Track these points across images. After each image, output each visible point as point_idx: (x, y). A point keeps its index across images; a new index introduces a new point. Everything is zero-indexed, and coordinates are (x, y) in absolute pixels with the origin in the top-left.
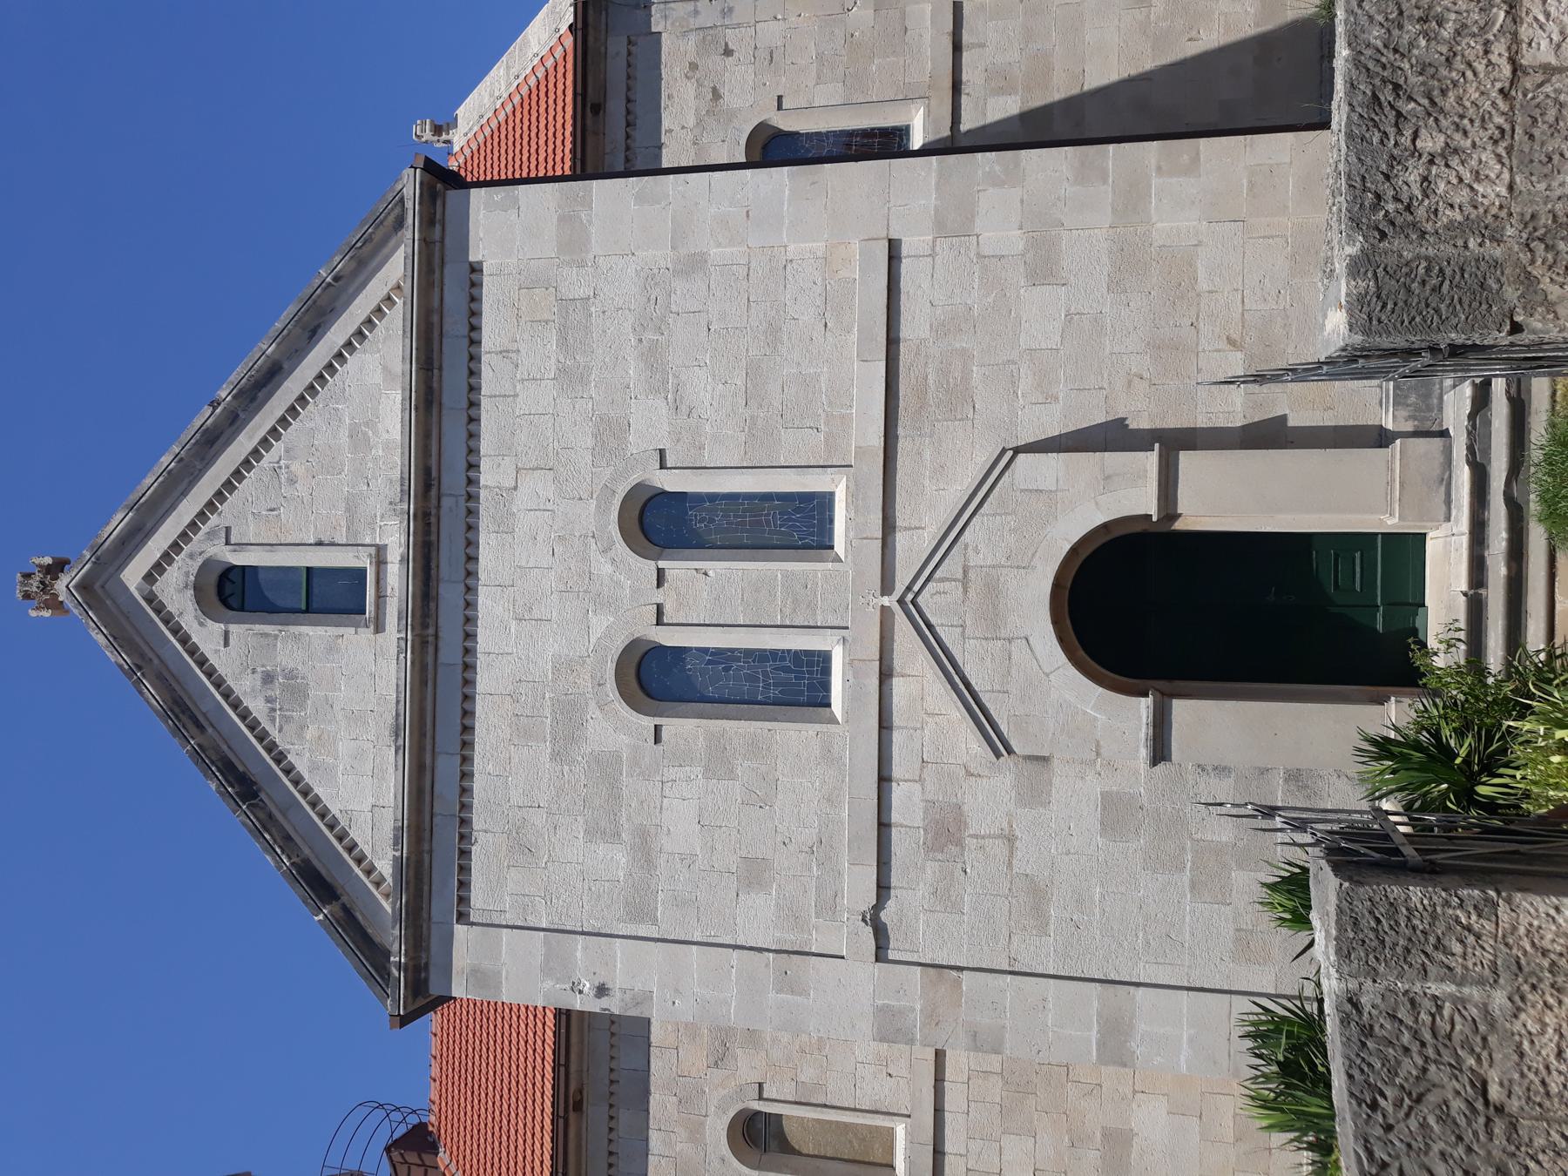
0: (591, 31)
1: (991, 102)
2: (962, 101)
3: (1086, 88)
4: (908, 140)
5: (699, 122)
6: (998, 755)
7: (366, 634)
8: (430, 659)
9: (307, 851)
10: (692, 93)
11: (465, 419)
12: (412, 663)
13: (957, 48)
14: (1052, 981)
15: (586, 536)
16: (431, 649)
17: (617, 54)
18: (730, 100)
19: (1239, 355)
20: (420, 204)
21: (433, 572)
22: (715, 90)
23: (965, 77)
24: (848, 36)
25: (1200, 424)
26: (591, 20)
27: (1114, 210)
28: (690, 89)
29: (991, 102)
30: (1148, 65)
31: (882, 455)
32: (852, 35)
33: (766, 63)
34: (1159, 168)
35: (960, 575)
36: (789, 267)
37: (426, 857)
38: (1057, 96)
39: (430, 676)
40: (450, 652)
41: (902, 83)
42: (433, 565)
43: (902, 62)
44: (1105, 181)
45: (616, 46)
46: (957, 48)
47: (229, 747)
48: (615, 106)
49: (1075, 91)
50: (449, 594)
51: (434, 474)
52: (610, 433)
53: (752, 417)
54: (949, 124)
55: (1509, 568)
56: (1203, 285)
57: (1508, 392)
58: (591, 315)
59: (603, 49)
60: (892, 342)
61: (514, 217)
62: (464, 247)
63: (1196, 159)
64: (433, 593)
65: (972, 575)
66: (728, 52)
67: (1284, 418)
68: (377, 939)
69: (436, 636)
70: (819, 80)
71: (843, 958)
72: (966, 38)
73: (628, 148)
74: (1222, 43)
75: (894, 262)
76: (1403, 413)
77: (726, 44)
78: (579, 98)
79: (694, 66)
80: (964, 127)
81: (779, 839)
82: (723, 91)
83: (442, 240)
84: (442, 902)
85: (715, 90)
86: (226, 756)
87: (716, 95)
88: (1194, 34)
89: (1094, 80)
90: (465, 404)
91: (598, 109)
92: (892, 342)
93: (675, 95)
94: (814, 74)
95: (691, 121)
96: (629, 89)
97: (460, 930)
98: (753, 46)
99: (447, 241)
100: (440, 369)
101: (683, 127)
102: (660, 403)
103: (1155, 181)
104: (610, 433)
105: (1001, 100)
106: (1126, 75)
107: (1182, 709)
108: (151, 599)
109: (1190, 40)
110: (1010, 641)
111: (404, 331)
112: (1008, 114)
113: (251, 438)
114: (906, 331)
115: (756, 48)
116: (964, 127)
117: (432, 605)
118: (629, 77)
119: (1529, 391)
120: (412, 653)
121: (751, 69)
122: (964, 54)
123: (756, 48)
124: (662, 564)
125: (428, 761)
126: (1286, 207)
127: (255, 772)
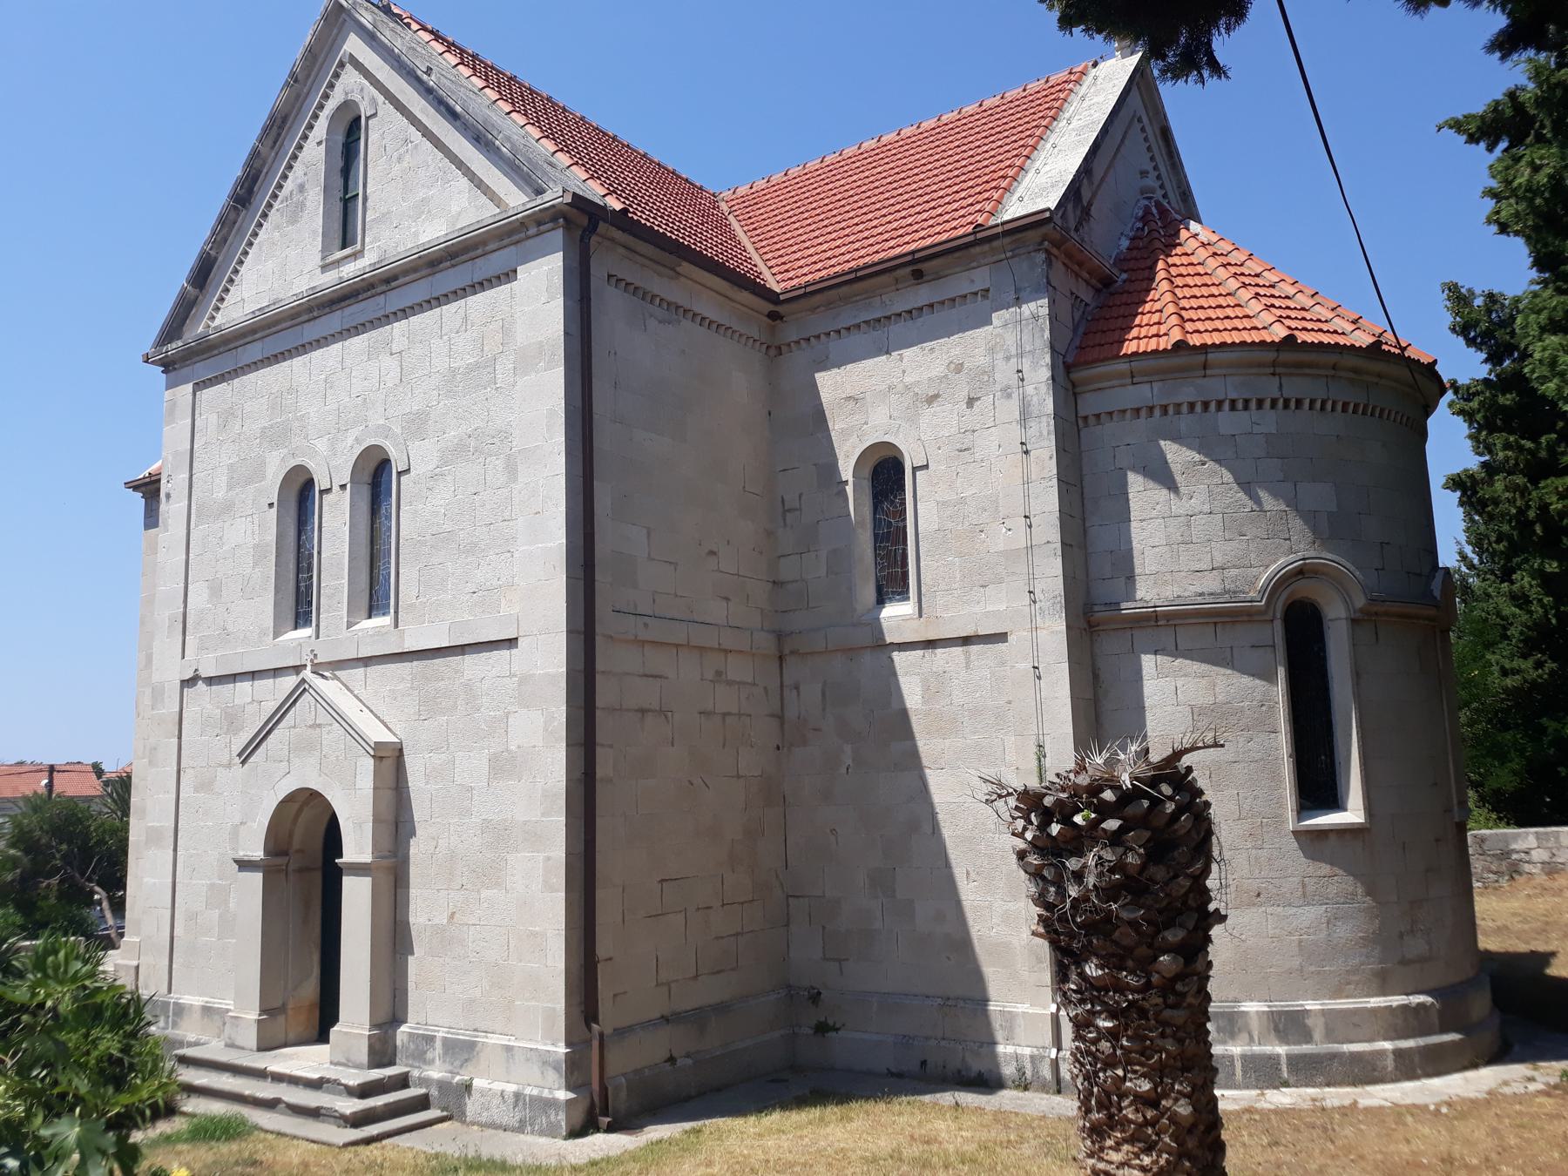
0: (986, 247)
1: (916, 679)
2: (918, 652)
3: (927, 771)
4: (899, 601)
5: (907, 388)
6: (239, 755)
7: (316, 259)
8: (284, 325)
9: (220, 259)
10: (934, 373)
11: (427, 298)
12: (292, 308)
13: (966, 641)
14: (174, 796)
15: (366, 421)
16: (289, 324)
17: (973, 281)
18: (927, 415)
19: (445, 921)
20: (540, 210)
21: (343, 304)
22: (936, 396)
23: (939, 651)
24: (981, 528)
25: (411, 890)
26: (996, 244)
27: (525, 823)
28: (938, 369)
29: (916, 679)
30: (947, 832)
31: (400, 651)
32: (982, 531)
33: (959, 446)
34: (549, 859)
35: (318, 722)
36: (509, 554)
37: (216, 352)
38: (920, 744)
39: (274, 329)
40: (311, 331)
41: (935, 589)
42: (347, 302)
43: (956, 586)
44: (543, 815)
45: (980, 278)
46: (966, 641)
47: (267, 173)
48: (922, 294)
49: (925, 762)
50: (334, 321)
51: (394, 284)
52: (417, 424)
53: (426, 541)
54: (896, 641)
55: (249, 1096)
56: (485, 893)
57: (322, 1108)
58: (485, 388)
59: (974, 264)
60: (462, 649)
61: (543, 300)
62: (526, 260)
63: (553, 890)
64: (334, 307)
65: (318, 729)
66: (971, 402)
67: (412, 954)
68: (184, 329)
69: (315, 318)
70: (942, 504)
71: (183, 658)
72: (974, 649)
73: (889, 318)
74: (964, 903)
75: (507, 643)
76: (406, 1039)
77: (979, 398)
78: (909, 258)
79: (959, 368)
80: (896, 656)
81: (229, 605)
82: (936, 407)
83: (528, 238)
84: (203, 369)
85: (936, 396)
86: (261, 172)
87: (932, 399)
88: (973, 875)
89: (934, 779)
90: (435, 295)
91: (918, 275)
92: (462, 649)
93: (934, 355)
94: (947, 498)
95: (908, 379)
96: (943, 303)
97: (189, 387)
98: (976, 428)
99: (531, 241)
100: (453, 266)
101: (904, 372)
102: (435, 462)
103: (541, 856)
104: (417, 424)
105: (918, 690)
106: (938, 810)
107: (258, 877)
108: (342, 65)
109: (968, 873)
110: (288, 761)
111: (462, 229)
112: (906, 696)
113: (422, 111)
114: (469, 659)
115: (974, 431)
116: (896, 656)
117: (327, 310)
118: (953, 300)
119: (323, 1122)
120: (298, 305)
121: (954, 430)
122: (960, 649)
123: (974, 431)
124: (348, 486)
125: (258, 336)
126: (521, 961)
127: (255, 201)
